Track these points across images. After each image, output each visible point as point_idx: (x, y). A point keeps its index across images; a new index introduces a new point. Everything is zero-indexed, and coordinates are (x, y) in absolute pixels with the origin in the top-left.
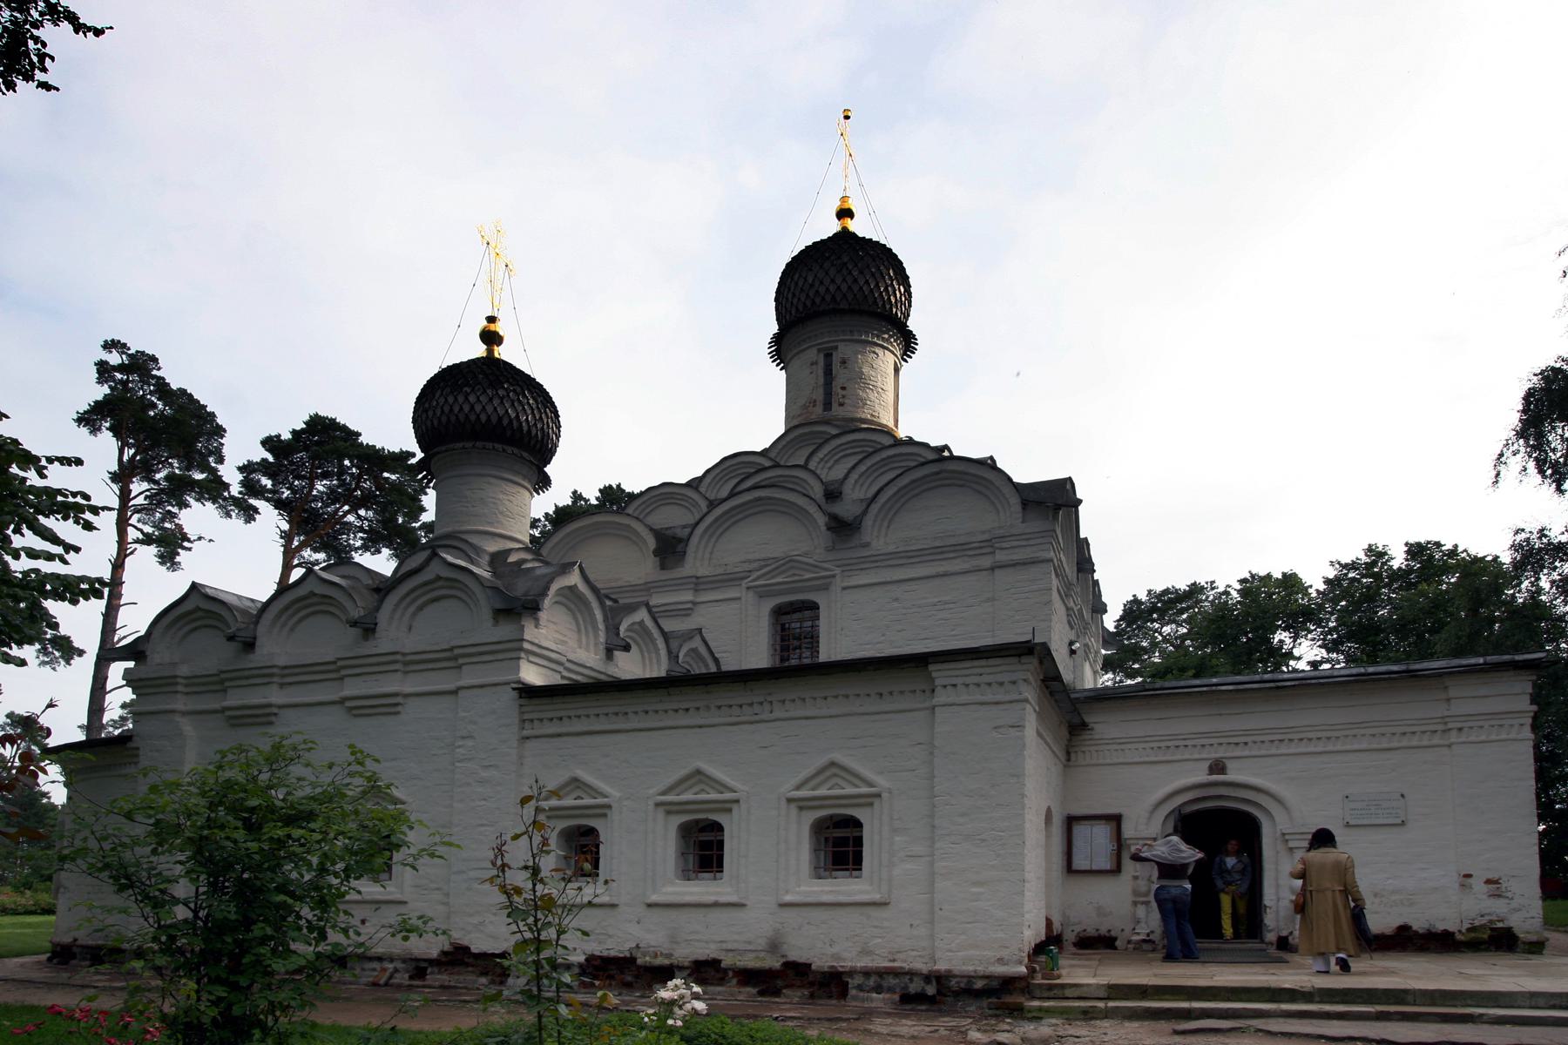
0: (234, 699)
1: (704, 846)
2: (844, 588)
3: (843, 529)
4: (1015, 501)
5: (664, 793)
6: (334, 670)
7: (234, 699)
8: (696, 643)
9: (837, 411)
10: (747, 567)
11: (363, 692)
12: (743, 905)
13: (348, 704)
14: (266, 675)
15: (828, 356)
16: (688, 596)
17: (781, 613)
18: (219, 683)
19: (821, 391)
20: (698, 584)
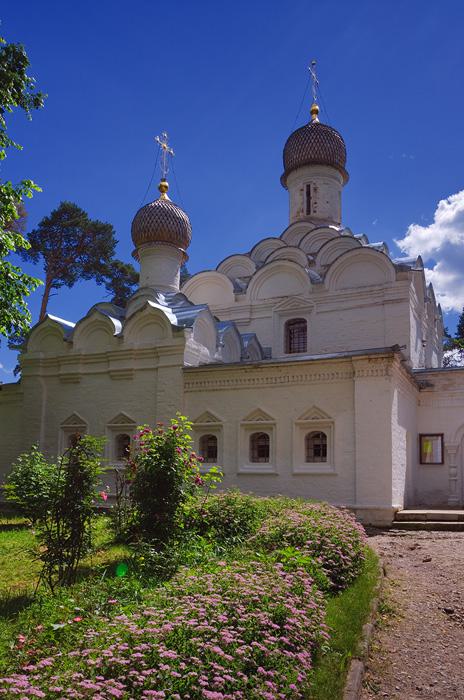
2: (318, 313)
4: (393, 270)
5: (244, 420)
12: (277, 475)
13: (112, 374)
14: (77, 359)
18: (58, 362)
19: (305, 204)
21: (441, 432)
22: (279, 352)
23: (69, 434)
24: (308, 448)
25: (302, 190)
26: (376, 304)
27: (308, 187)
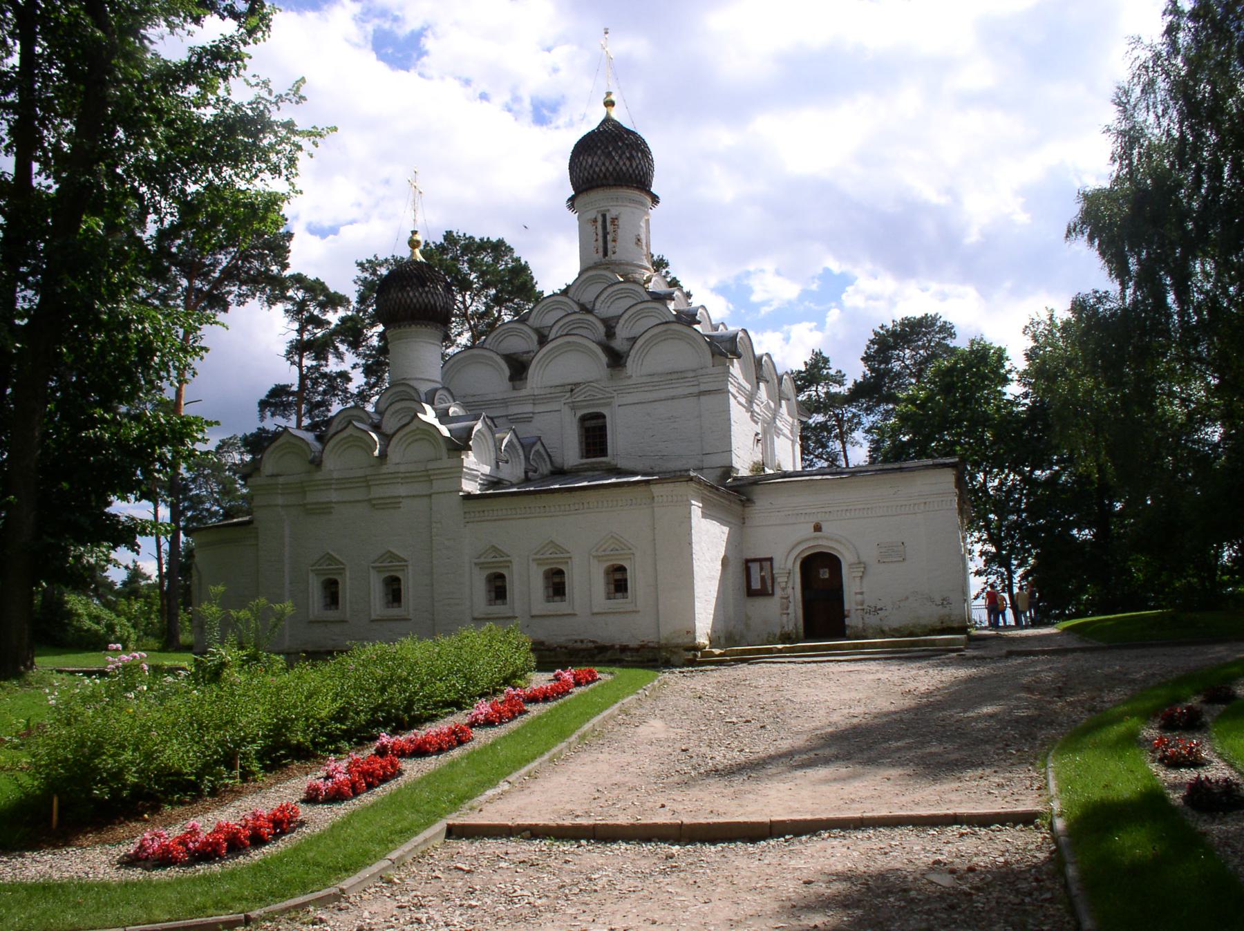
0: (377, 492)
1: (497, 588)
3: (616, 359)
7: (377, 492)
12: (575, 615)
16: (528, 408)
20: (535, 399)
22: (571, 455)
23: (323, 578)
24: (608, 584)
25: (595, 221)
27: (604, 216)
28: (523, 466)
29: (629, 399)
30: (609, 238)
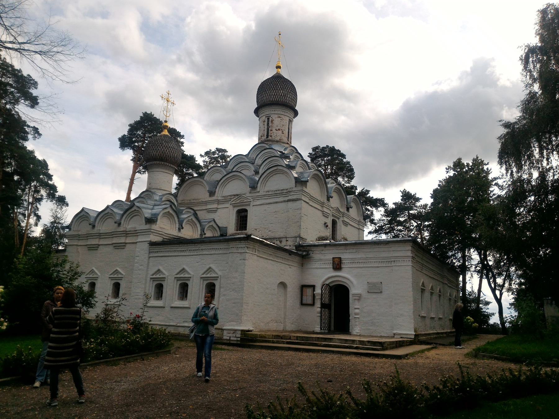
5: (176, 275)
6: (112, 235)
8: (213, 223)
9: (270, 138)
10: (230, 197)
11: (117, 242)
12: (164, 307)
14: (100, 236)
15: (268, 119)
16: (215, 206)
17: (239, 212)
19: (266, 131)
20: (218, 202)
21: (312, 284)
26: (284, 201)
28: (199, 233)
29: (258, 202)
30: (270, 129)
